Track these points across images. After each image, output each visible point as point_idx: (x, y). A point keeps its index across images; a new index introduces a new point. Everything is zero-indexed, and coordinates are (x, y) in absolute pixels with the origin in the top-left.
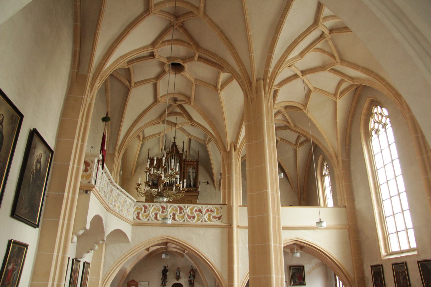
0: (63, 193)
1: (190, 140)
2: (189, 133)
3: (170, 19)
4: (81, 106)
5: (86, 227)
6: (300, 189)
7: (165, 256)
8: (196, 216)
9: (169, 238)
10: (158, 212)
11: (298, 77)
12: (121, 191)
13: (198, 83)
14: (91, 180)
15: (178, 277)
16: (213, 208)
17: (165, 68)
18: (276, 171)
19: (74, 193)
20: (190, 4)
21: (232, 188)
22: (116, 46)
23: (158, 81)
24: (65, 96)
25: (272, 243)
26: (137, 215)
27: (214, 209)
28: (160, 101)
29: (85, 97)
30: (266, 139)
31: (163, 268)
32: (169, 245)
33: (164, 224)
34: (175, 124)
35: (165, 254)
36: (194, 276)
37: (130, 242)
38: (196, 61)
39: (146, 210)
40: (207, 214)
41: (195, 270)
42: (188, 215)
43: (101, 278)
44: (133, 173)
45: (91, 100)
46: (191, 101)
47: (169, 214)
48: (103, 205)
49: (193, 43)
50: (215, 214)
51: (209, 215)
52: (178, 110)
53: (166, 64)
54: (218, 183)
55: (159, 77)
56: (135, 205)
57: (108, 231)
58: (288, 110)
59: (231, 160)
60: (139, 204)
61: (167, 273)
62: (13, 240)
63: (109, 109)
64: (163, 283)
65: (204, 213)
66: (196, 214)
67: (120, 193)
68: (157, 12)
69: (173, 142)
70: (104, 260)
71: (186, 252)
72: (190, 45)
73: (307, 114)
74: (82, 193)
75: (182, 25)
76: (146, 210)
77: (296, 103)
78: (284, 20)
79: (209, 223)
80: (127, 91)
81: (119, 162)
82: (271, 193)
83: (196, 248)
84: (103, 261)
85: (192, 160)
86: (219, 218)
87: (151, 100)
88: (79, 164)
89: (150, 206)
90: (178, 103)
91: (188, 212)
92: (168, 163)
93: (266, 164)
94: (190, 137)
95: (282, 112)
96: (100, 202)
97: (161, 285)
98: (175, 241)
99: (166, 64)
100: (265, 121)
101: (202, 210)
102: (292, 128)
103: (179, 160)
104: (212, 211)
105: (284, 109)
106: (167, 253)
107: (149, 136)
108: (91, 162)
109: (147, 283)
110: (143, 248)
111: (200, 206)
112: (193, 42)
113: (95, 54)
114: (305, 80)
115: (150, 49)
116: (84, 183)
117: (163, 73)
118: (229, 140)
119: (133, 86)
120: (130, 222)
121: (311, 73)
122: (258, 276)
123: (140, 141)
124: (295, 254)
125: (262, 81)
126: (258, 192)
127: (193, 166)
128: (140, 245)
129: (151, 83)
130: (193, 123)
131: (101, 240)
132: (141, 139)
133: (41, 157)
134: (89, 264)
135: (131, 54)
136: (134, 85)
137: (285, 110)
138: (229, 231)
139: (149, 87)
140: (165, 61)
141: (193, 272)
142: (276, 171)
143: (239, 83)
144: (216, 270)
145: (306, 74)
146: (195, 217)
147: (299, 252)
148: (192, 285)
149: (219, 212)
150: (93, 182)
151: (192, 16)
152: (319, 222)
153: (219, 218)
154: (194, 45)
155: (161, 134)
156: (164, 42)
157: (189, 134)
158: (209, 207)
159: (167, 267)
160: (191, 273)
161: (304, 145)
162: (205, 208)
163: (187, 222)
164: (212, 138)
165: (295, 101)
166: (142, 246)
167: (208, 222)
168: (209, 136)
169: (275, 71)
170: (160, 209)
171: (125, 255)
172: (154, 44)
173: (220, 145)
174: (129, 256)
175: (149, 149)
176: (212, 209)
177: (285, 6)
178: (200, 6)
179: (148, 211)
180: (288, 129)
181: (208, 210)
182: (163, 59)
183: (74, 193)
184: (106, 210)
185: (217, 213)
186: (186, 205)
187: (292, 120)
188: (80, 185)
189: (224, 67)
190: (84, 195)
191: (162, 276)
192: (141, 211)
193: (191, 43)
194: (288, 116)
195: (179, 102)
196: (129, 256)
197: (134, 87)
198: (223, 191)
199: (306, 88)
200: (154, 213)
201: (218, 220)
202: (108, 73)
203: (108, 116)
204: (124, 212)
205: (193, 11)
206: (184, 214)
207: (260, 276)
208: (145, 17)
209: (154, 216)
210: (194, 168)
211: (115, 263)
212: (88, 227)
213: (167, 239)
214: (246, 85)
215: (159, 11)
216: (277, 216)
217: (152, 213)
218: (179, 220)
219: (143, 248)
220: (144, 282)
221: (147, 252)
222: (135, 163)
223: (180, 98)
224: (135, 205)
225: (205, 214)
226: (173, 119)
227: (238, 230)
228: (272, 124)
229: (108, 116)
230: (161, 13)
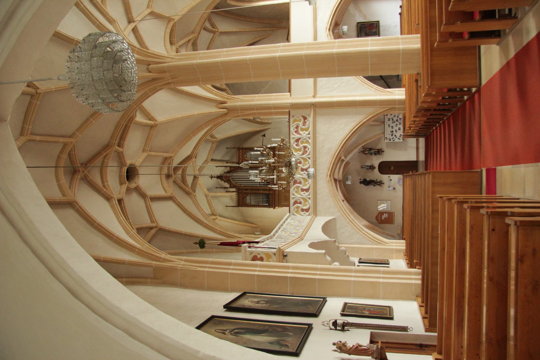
0: (289, 278)
1: (212, 160)
2: (205, 161)
3: (78, 179)
4: (190, 270)
5: (323, 253)
6: (268, 28)
7: (349, 181)
8: (303, 145)
9: (329, 174)
10: (300, 189)
11: (136, 28)
12: (279, 228)
13: (148, 148)
14: (272, 252)
15: (372, 168)
16: (293, 126)
17: (133, 187)
18: (254, 49)
19: (288, 267)
20: (60, 155)
21: (270, 104)
22: (116, 237)
23: (148, 195)
24: (179, 288)
25: (335, 51)
26: (305, 212)
27: (295, 125)
28: (171, 194)
29: (179, 266)
30: (218, 60)
31: (361, 184)
32: (336, 177)
33: (315, 176)
34: (195, 177)
35: (347, 180)
36: (370, 149)
37: (335, 217)
38: (123, 150)
39: (298, 201)
40: (301, 132)
41: (363, 148)
42: (303, 154)
43: (375, 246)
44: (254, 225)
45: (182, 260)
46: (169, 156)
48: (297, 243)
49: (105, 152)
50: (301, 124)
51: (302, 130)
52: (180, 172)
53: (128, 185)
54: (263, 125)
55: (143, 195)
56: (294, 215)
57: (325, 238)
58: (175, 40)
59: (238, 107)
60: (292, 210)
61: (368, 180)
62: (341, 313)
63: (185, 251)
64: (378, 183)
65: (299, 136)
66: (301, 144)
67: (281, 230)
68: (72, 193)
69: (217, 179)
70: (355, 244)
71: (343, 158)
72: (107, 155)
73: (179, 17)
74: (287, 260)
75: (84, 165)
76: (298, 202)
77: (167, 30)
78: (76, 39)
79: (311, 129)
81: (244, 236)
82: (280, 53)
83: (340, 143)
84: (356, 246)
85: (237, 157)
86: (305, 118)
87: (170, 204)
88: (256, 266)
89: (294, 198)
90: (172, 172)
91: (298, 154)
92: (242, 183)
93: (248, 59)
94: (209, 160)
95: (177, 48)
96: (294, 245)
97: (381, 186)
98: (332, 167)
99: (128, 186)
100: (199, 61)
101: (296, 138)
102: (195, 36)
103: (238, 170)
104: (297, 127)
105: (174, 45)
106: (345, 178)
107: (210, 208)
108: (252, 254)
109: (379, 202)
110: (341, 203)
111: (292, 141)
112: (103, 152)
113: (128, 260)
114: (139, 18)
115: (114, 202)
116: (275, 260)
117: (138, 190)
118: (213, 110)
119: (156, 225)
120: (313, 218)
121: (131, 11)
122: (369, 66)
123: (217, 218)
124: (345, 31)
125: (151, 66)
126: (279, 67)
127: (244, 153)
128: (338, 206)
129: (150, 203)
130: (194, 155)
131: (335, 244)
132: (214, 217)
133: (252, 301)
134: (360, 259)
135: (123, 222)
136: (155, 223)
137: (175, 45)
138: (319, 107)
139: (156, 206)
140: (124, 187)
141: (366, 150)
142: (254, 49)
143: (152, 94)
144: (363, 120)
145: (132, 17)
146: (305, 146)
147: (342, 27)
148: (380, 151)
149: (298, 119)
150: (275, 250)
151: (75, 151)
152: (309, 2)
153: (305, 118)
154: (107, 150)
155: (207, 194)
156: (104, 186)
157: (206, 162)
159: (360, 181)
160: (366, 152)
161: (215, 23)
162: (293, 134)
163: (310, 154)
164: (210, 133)
166: (339, 204)
167: (310, 131)
168: (207, 136)
169: (137, 51)
170: (297, 186)
171: (350, 222)
172: (108, 198)
173: (220, 121)
174: (350, 217)
175: (227, 206)
176: (294, 127)
177: (57, 38)
178: (62, 143)
179: (299, 200)
180: (197, 41)
181: (296, 132)
182: (123, 189)
183: (288, 267)
184: (302, 240)
185: (300, 121)
186: (292, 196)
187: (186, 36)
188: (278, 262)
189: (130, 116)
190: (288, 258)
191: (371, 185)
192: (300, 208)
193: (105, 154)
194: (181, 41)
195: (171, 172)
196: (350, 217)
197: (157, 223)
198: (273, 115)
199: (148, 18)
200: (302, 193)
201: (307, 120)
202: (149, 246)
203: (198, 242)
204: (303, 225)
205: (68, 152)
207: (369, 63)
208: (80, 207)
209: (305, 192)
210: (246, 153)
211: (358, 233)
212: (323, 251)
213: (330, 176)
214: (155, 85)
215: (71, 191)
216: (305, 46)
217: (302, 195)
218: (309, 164)
219: (341, 203)
221: (345, 201)
222: (243, 223)
223: (165, 171)
224: (294, 215)
225: (301, 135)
226: (189, 180)
228: (200, 54)
229: (198, 242)
230: (72, 189)
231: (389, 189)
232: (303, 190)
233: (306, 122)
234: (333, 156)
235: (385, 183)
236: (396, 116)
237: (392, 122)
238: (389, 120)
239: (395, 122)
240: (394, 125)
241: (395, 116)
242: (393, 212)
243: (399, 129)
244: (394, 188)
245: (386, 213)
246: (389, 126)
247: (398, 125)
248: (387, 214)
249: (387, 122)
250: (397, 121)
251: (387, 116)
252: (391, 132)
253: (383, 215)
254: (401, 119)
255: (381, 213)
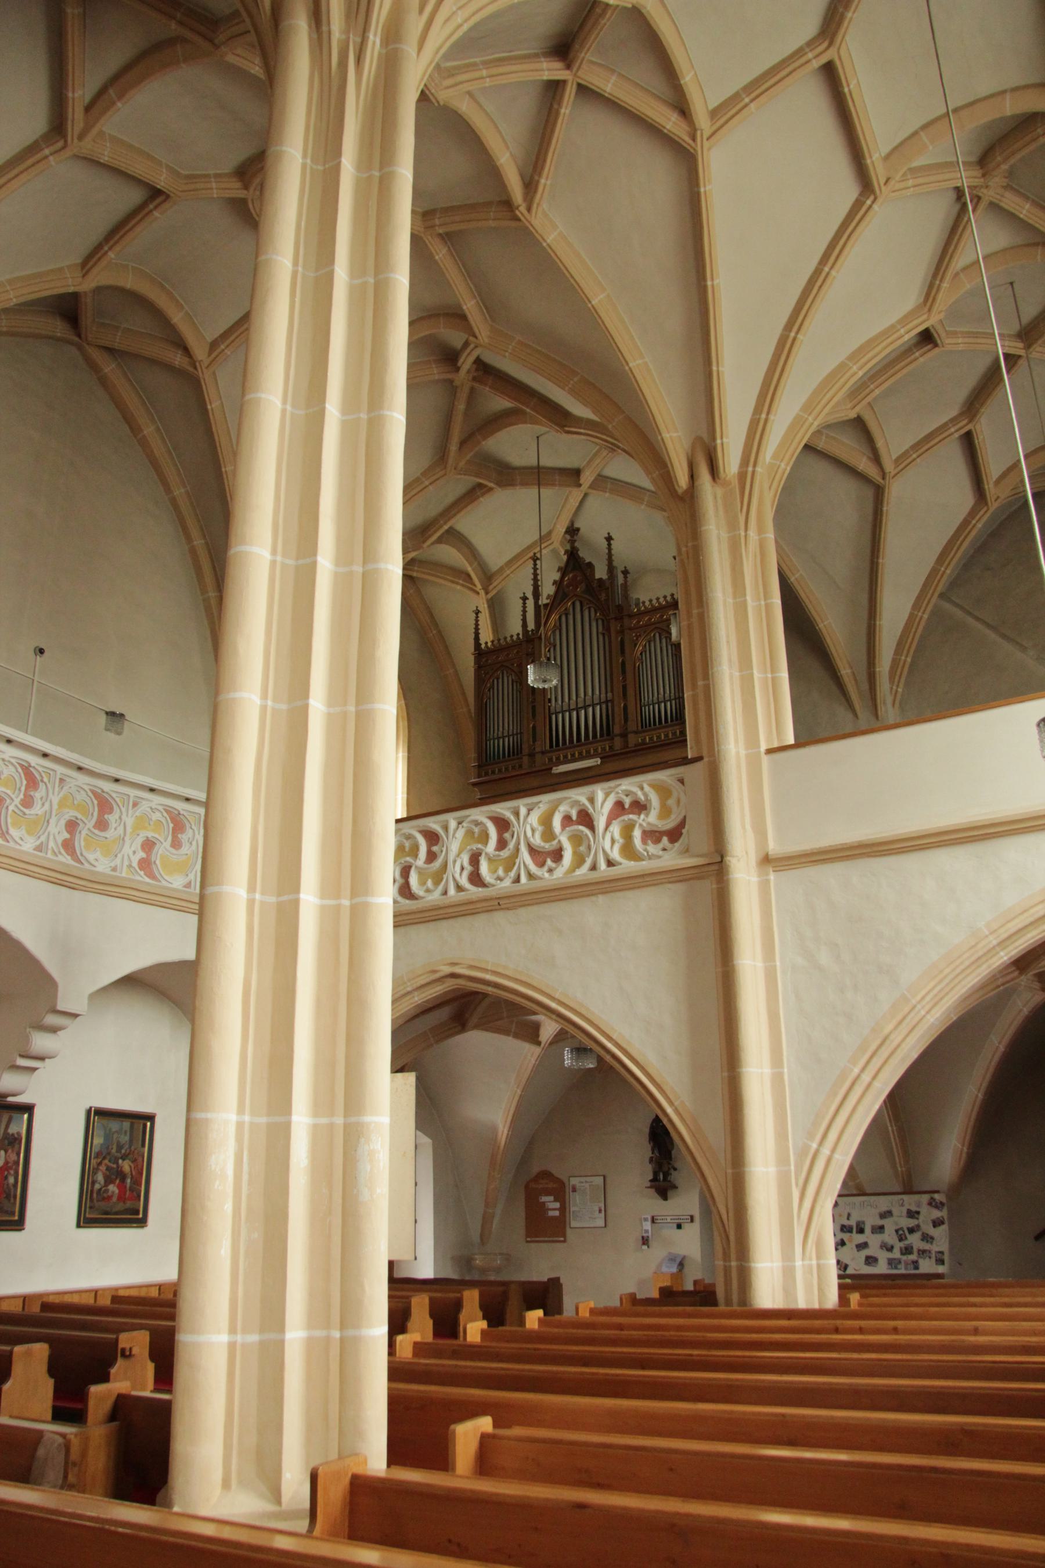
16: (642, 788)
27: (646, 795)
42: (532, 850)
47: (455, 862)
50: (652, 818)
52: (501, 403)
65: (601, 823)
79: (628, 866)
80: (195, 384)
86: (675, 835)
104: (639, 807)
123: (478, 593)
137: (984, 175)
149: (671, 802)
153: (675, 835)
158: (623, 787)
165: (1000, 89)
181: (619, 804)
186: (522, 805)
200: (465, 859)
206: (517, 850)
213: (453, 976)
220: (588, 1179)
227: (768, 881)
231: (646, 1220)
232: (475, 859)
233: (657, 841)
234: (523, 979)
235: (669, 1201)
236: (925, 1246)
237: (902, 1229)
238: (912, 1214)
239: (901, 1240)
240: (889, 1236)
241: (927, 1238)
242: (564, 1236)
243: (871, 1260)
244: (647, 1240)
245: (563, 1209)
246: (886, 1214)
247: (890, 1255)
248: (557, 1213)
249: (902, 1205)
250: (907, 1250)
251: (930, 1204)
252: (858, 1224)
253: (555, 1200)
254: (917, 1268)
255: (560, 1191)
